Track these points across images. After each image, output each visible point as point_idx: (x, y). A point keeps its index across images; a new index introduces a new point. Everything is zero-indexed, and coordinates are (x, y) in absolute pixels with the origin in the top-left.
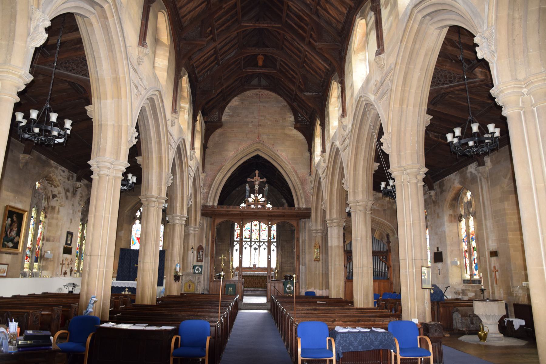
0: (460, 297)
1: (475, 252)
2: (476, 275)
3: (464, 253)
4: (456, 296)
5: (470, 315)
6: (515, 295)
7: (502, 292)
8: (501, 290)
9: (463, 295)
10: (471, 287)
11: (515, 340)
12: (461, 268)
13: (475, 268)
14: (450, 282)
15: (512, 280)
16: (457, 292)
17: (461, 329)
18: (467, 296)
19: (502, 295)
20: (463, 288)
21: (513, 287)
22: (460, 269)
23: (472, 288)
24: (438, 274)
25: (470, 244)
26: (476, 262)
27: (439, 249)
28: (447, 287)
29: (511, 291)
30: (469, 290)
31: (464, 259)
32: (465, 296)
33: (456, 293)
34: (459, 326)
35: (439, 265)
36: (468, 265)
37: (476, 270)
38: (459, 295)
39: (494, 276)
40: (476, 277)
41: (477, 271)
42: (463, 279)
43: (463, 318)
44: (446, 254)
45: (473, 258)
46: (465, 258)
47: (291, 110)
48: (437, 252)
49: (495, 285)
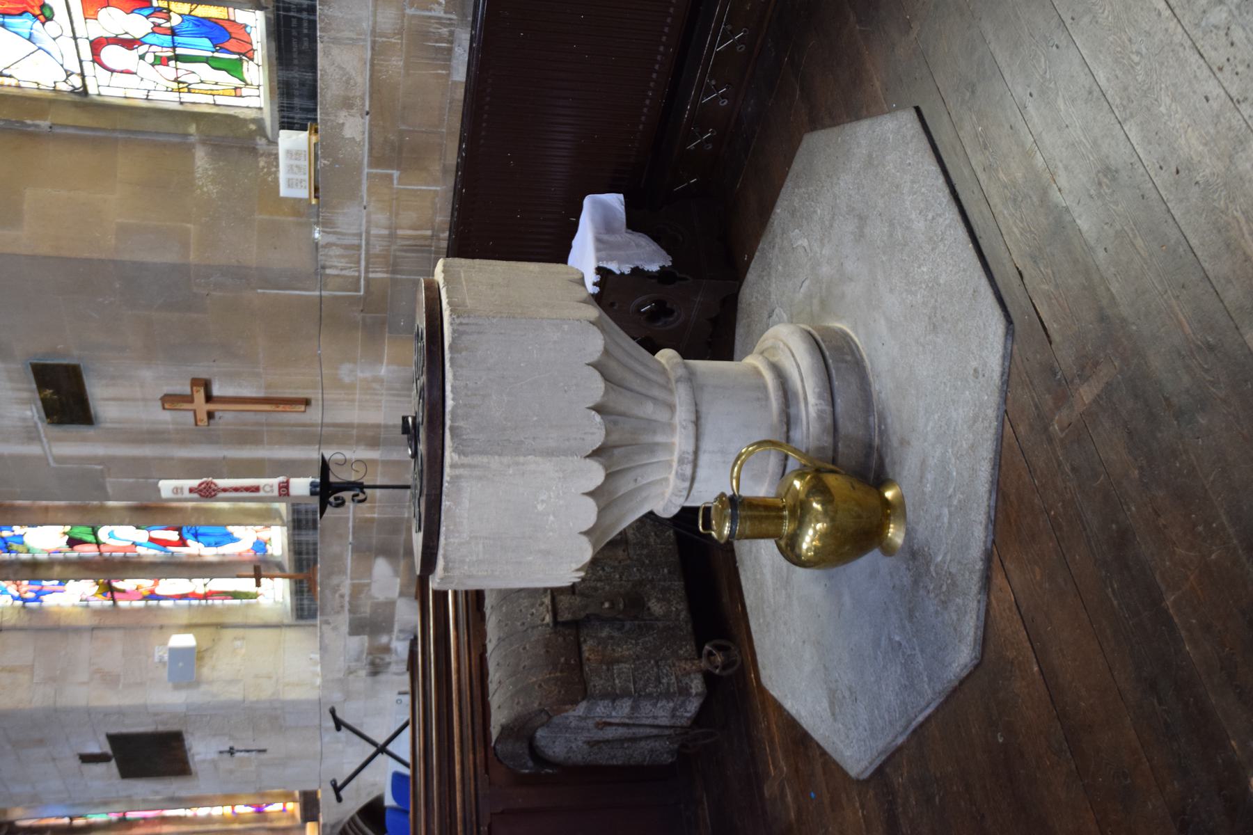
0: (401, 648)
1: (103, 533)
2: (260, 546)
3: (123, 604)
4: (393, 668)
5: (565, 616)
6: (379, 275)
7: (364, 373)
8: (346, 372)
9: (388, 629)
10: (335, 580)
11: (934, 168)
12: (223, 626)
13: (217, 544)
14: (314, 695)
15: (267, 279)
16: (373, 664)
17: (693, 706)
18: (391, 604)
19: (383, 371)
20: (345, 629)
21: (319, 274)
22: (228, 634)
23: (342, 572)
24: (263, 756)
25: (50, 564)
26: (173, 536)
27: (94, 749)
28: (339, 724)
29: (353, 301)
30: (357, 591)
31: (163, 603)
32: (392, 616)
33: (376, 669)
34: (664, 721)
35: (201, 749)
36: (198, 585)
37: (231, 539)
38: (387, 649)
39: (251, 415)
40: (277, 540)
41: (235, 530)
42: (289, 619)
43: (597, 683)
44: (121, 712)
45: (149, 553)
46: (153, 596)
47: (768, 225)
48: (113, 763)
49: (313, 415)
